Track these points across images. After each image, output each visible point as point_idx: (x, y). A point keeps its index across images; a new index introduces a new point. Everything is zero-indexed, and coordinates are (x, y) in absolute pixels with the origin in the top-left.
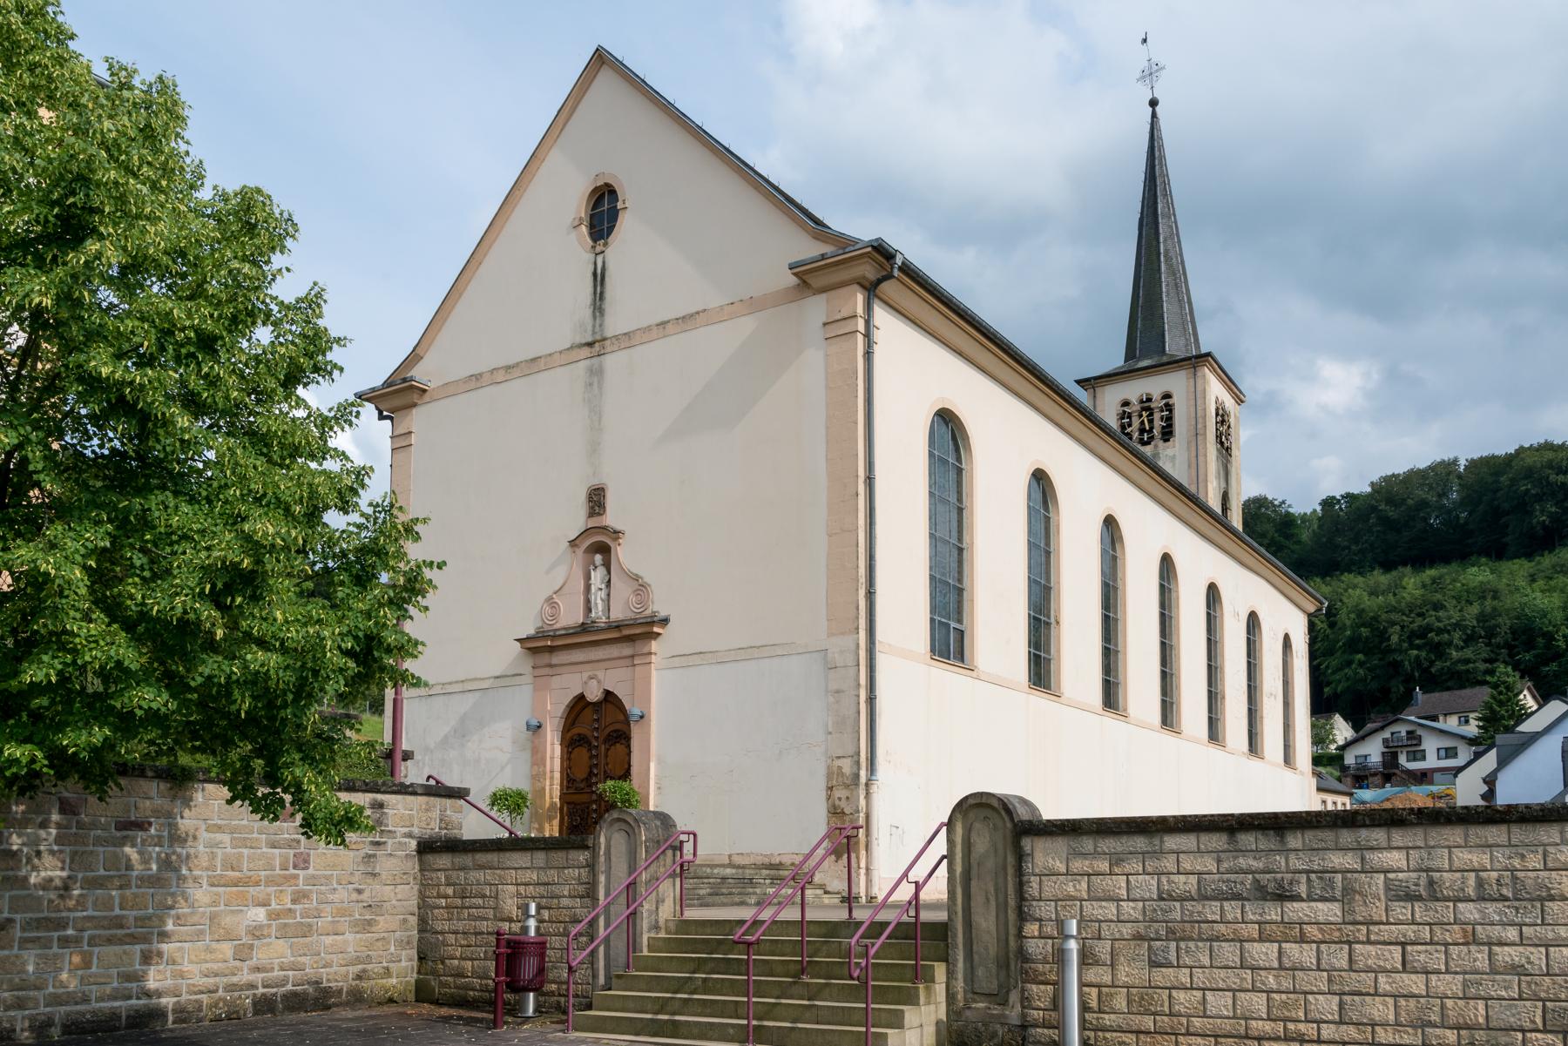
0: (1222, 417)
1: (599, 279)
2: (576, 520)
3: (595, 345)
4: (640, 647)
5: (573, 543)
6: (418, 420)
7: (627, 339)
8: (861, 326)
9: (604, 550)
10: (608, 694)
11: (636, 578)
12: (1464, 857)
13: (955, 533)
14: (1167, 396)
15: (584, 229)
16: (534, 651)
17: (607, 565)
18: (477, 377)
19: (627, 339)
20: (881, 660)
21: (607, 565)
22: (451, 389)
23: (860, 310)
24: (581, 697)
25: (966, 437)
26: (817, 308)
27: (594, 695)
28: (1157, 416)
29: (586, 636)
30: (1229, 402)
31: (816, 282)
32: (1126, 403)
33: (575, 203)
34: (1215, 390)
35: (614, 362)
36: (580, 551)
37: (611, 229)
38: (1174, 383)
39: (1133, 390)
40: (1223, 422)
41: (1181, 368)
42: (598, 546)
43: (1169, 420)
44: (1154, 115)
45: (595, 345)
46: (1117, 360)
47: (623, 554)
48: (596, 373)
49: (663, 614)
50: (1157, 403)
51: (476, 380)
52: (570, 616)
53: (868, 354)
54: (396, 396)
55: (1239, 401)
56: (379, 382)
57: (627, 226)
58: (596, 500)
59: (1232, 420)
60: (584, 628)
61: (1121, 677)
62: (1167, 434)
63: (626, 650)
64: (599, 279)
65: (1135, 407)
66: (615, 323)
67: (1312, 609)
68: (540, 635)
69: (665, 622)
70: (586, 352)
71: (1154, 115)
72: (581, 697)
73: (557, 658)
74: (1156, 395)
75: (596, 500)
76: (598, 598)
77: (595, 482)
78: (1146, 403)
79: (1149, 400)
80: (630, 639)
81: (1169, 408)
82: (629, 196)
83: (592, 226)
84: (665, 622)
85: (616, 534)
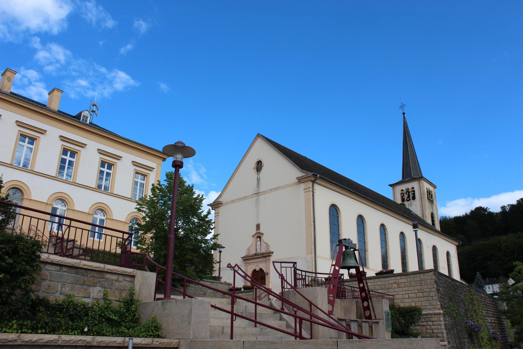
0: (429, 193)
1: (258, 180)
2: (254, 231)
3: (258, 194)
4: (267, 258)
5: (253, 236)
6: (221, 209)
7: (264, 192)
8: (311, 189)
9: (260, 237)
10: (261, 269)
11: (266, 243)
12: (379, 283)
13: (337, 231)
14: (413, 188)
15: (256, 170)
16: (245, 260)
17: (260, 240)
18: (233, 201)
19: (264, 192)
20: (318, 260)
21: (260, 240)
22: (227, 203)
23: (311, 186)
24: (255, 270)
25: (339, 210)
26: (302, 186)
27: (258, 269)
28: (411, 194)
29: (257, 256)
30: (431, 188)
31: (302, 181)
32: (402, 190)
33: (253, 164)
34: (426, 186)
35: (261, 197)
36: (255, 238)
37: (261, 169)
38: (414, 185)
39: (404, 187)
40: (430, 194)
41: (416, 181)
42: (259, 236)
43: (414, 194)
44: (404, 116)
45: (258, 194)
46: (400, 179)
47: (264, 238)
48: (258, 200)
49: (272, 251)
50: (410, 190)
51: (233, 201)
52: (253, 252)
53: (313, 195)
54: (216, 205)
55: (435, 187)
56: (212, 202)
57: (264, 169)
58: (258, 227)
59: (433, 193)
60: (256, 255)
61: (389, 264)
62: (414, 198)
63: (264, 259)
64: (258, 180)
65: (405, 191)
66: (262, 190)
67: (457, 244)
68: (246, 256)
69: (273, 253)
70: (256, 195)
71: (404, 116)
72: (255, 270)
73: (250, 261)
74: (410, 188)
75: (258, 227)
76: (258, 248)
77: (258, 223)
78: (408, 191)
79: (408, 189)
80: (265, 257)
81: (414, 191)
82: (264, 162)
83: (257, 169)
84: (273, 253)
85: (262, 234)
